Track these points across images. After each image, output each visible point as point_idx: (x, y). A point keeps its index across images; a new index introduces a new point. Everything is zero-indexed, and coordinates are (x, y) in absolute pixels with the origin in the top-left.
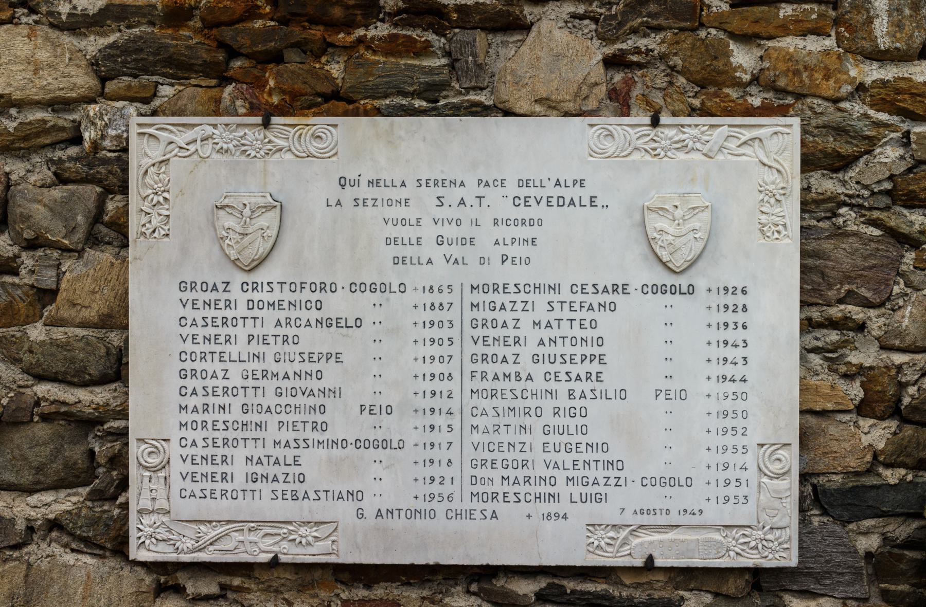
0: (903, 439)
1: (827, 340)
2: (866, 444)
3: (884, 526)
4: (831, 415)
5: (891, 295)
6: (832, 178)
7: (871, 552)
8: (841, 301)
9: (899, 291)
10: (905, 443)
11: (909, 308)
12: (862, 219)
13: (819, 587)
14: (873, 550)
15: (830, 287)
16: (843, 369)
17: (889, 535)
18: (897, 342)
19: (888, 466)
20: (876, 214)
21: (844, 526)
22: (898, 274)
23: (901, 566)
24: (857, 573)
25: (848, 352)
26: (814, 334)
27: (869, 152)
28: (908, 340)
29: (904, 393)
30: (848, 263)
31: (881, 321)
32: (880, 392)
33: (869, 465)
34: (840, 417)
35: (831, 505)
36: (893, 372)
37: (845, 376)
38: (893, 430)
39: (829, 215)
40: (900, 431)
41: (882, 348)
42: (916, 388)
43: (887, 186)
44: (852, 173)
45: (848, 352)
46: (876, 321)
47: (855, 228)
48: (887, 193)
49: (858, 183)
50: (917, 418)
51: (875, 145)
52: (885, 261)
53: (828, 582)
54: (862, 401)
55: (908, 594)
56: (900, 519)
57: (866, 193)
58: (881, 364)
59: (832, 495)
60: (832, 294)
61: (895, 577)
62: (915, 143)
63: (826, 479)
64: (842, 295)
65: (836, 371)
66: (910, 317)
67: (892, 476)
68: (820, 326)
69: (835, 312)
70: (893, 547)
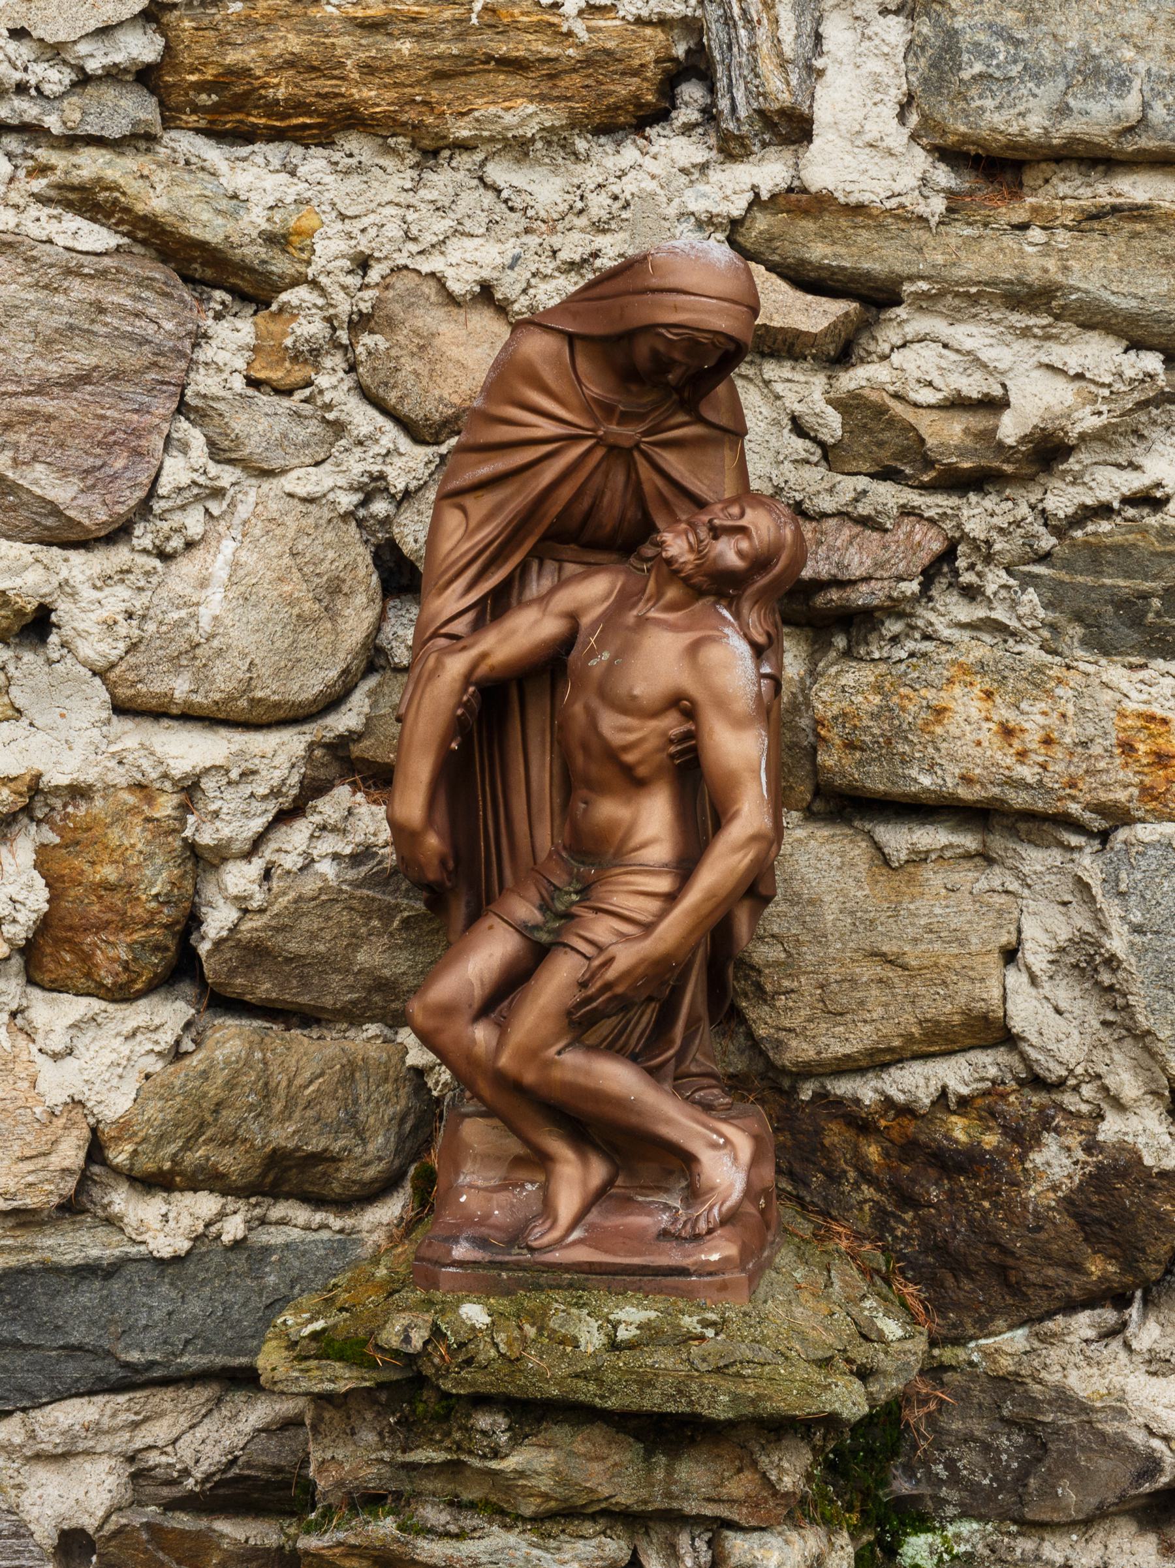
0: (204, 1075)
2: (57, 1097)
5: (152, 493)
9: (184, 479)
10: (214, 1090)
11: (228, 547)
12: (38, 185)
14: (89, 1523)
17: (154, 1458)
18: (180, 687)
20: (90, 164)
22: (183, 409)
28: (224, 679)
29: (210, 891)
31: (117, 599)
32: (111, 888)
33: (70, 1185)
36: (166, 806)
38: (166, 1039)
41: (121, 709)
42: (256, 867)
43: (142, 47)
46: (93, 598)
48: (145, 77)
50: (265, 989)
52: (131, 357)
54: (44, 925)
56: (199, 1396)
57: (55, 78)
58: (119, 776)
66: (232, 582)
67: (162, 1225)
70: (171, 1506)
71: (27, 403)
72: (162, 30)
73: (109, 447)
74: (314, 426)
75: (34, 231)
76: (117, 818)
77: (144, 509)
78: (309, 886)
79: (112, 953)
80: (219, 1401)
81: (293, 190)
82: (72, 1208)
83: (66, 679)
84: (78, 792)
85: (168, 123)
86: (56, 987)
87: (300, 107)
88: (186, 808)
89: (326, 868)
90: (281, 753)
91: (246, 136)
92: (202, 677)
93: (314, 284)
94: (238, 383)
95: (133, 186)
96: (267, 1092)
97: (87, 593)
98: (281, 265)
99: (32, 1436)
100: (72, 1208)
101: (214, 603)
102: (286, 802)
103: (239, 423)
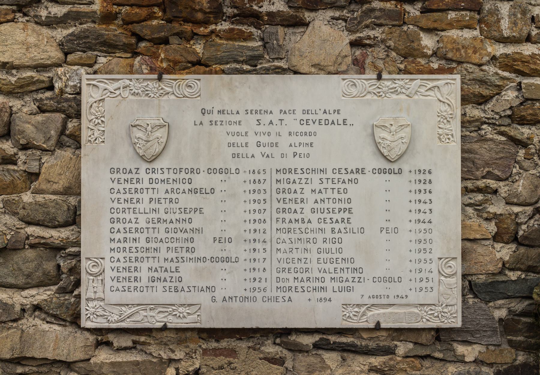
0: (519, 255)
1: (476, 199)
2: (499, 257)
5: (512, 174)
6: (478, 108)
7: (502, 319)
8: (483, 177)
10: (520, 257)
11: (522, 181)
12: (495, 131)
13: (473, 338)
14: (503, 317)
16: (485, 215)
17: (512, 309)
18: (515, 200)
19: (511, 270)
20: (503, 129)
21: (487, 304)
22: (515, 162)
23: (519, 326)
24: (494, 331)
25: (488, 206)
26: (468, 196)
27: (498, 94)
28: (522, 199)
29: (519, 229)
31: (507, 188)
32: (506, 228)
34: (484, 242)
35: (479, 292)
36: (513, 217)
37: (486, 219)
38: (514, 249)
39: (476, 129)
40: (518, 250)
42: (526, 226)
43: (509, 112)
44: (489, 106)
45: (488, 206)
46: (503, 188)
47: (491, 136)
48: (509, 116)
49: (492, 111)
50: (527, 243)
51: (502, 90)
52: (508, 155)
54: (496, 233)
55: (523, 342)
56: (518, 300)
57: (497, 117)
58: (507, 213)
59: (480, 286)
60: (479, 173)
61: (516, 332)
62: (524, 89)
63: (476, 277)
64: (484, 174)
66: (522, 186)
67: (513, 276)
68: (472, 191)
69: (481, 183)
70: (514, 315)
71: (494, 161)
74: (533, 164)
78: (534, 228)
80: (521, 301)
81: (531, 132)
84: (501, 215)
87: (532, 120)
89: (536, 226)
91: (523, 124)
93: (534, 145)
95: (509, 132)
97: (502, 187)
98: (529, 142)
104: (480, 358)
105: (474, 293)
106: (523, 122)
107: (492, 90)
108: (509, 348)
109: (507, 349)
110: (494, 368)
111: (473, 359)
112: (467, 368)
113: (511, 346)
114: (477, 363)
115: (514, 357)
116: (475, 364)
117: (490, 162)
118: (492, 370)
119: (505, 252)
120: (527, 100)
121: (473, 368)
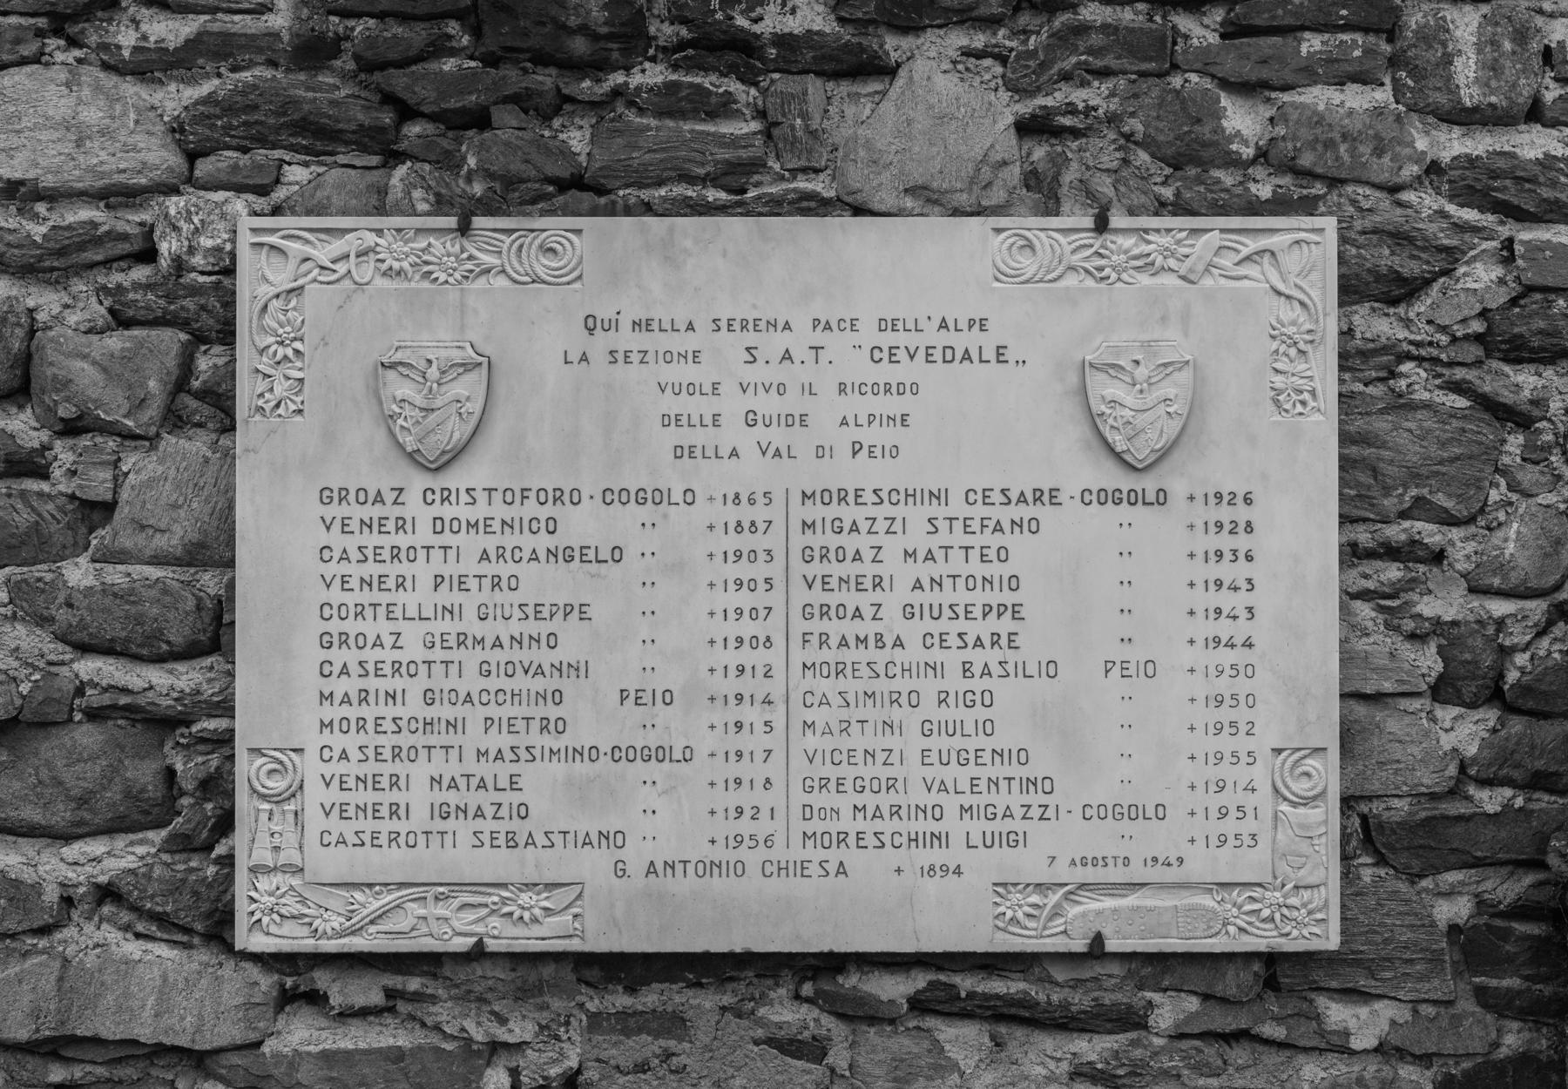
1: (1383, 578)
2: (1447, 747)
3: (1478, 882)
4: (1389, 700)
5: (1485, 504)
6: (1387, 315)
7: (1457, 925)
8: (1404, 515)
10: (1511, 746)
11: (1515, 525)
12: (1437, 382)
13: (1373, 983)
14: (1461, 922)
15: (1387, 491)
16: (1409, 625)
17: (1486, 896)
18: (1496, 582)
19: (1484, 783)
20: (1460, 373)
22: (1497, 470)
24: (1435, 960)
25: (1416, 597)
26: (1360, 569)
28: (1515, 578)
29: (1508, 665)
30: (1415, 453)
31: (1471, 547)
32: (1468, 663)
33: (1453, 782)
34: (1404, 703)
35: (1392, 849)
36: (1491, 630)
37: (1412, 637)
38: (1491, 724)
39: (1383, 374)
41: (1472, 590)
42: (1527, 655)
43: (1477, 327)
44: (1421, 307)
45: (1416, 597)
46: (1462, 547)
47: (1426, 396)
48: (1478, 338)
49: (1429, 322)
50: (1530, 704)
51: (1457, 260)
52: (1475, 449)
53: (1388, 975)
54: (1441, 677)
55: (1519, 993)
56: (1504, 871)
57: (1444, 339)
58: (1471, 618)
60: (1390, 504)
61: (1498, 965)
62: (1522, 257)
63: (1383, 806)
64: (1407, 505)
65: (1397, 629)
66: (1517, 540)
67: (1490, 800)
68: (1371, 555)
69: (1396, 533)
70: (1493, 916)
72: (1486, 320)
73: (1468, 486)
74: (1549, 477)
75: (1437, 400)
76: (1471, 634)
77: (1482, 511)
78: (1550, 663)
79: (1469, 689)
80: (1512, 873)
82: (1454, 792)
83: (1451, 578)
84: (1455, 623)
85: (1488, 356)
86: (1445, 702)
87: (1544, 349)
88: (1498, 631)
89: (1556, 655)
90: (1537, 609)
91: (1517, 361)
92: (1505, 578)
93: (1550, 420)
94: (1518, 460)
95: (1477, 382)
96: (1533, 747)
97: (1459, 544)
98: (1536, 413)
99: (1437, 885)
100: (1454, 792)
101: (1511, 547)
102: (1540, 629)
103: (1519, 476)
104: (1395, 1040)
105: (1377, 852)
106: (1518, 353)
107: (1428, 263)
108: (1478, 1009)
109: (1473, 1014)
110: (1435, 1069)
111: (1374, 1043)
112: (1356, 1068)
113: (1485, 1006)
114: (1384, 1054)
115: (1494, 1035)
116: (1380, 1058)
117: (1424, 471)
118: (1428, 1073)
119: (1465, 731)
120: (1530, 289)
121: (1375, 1067)
